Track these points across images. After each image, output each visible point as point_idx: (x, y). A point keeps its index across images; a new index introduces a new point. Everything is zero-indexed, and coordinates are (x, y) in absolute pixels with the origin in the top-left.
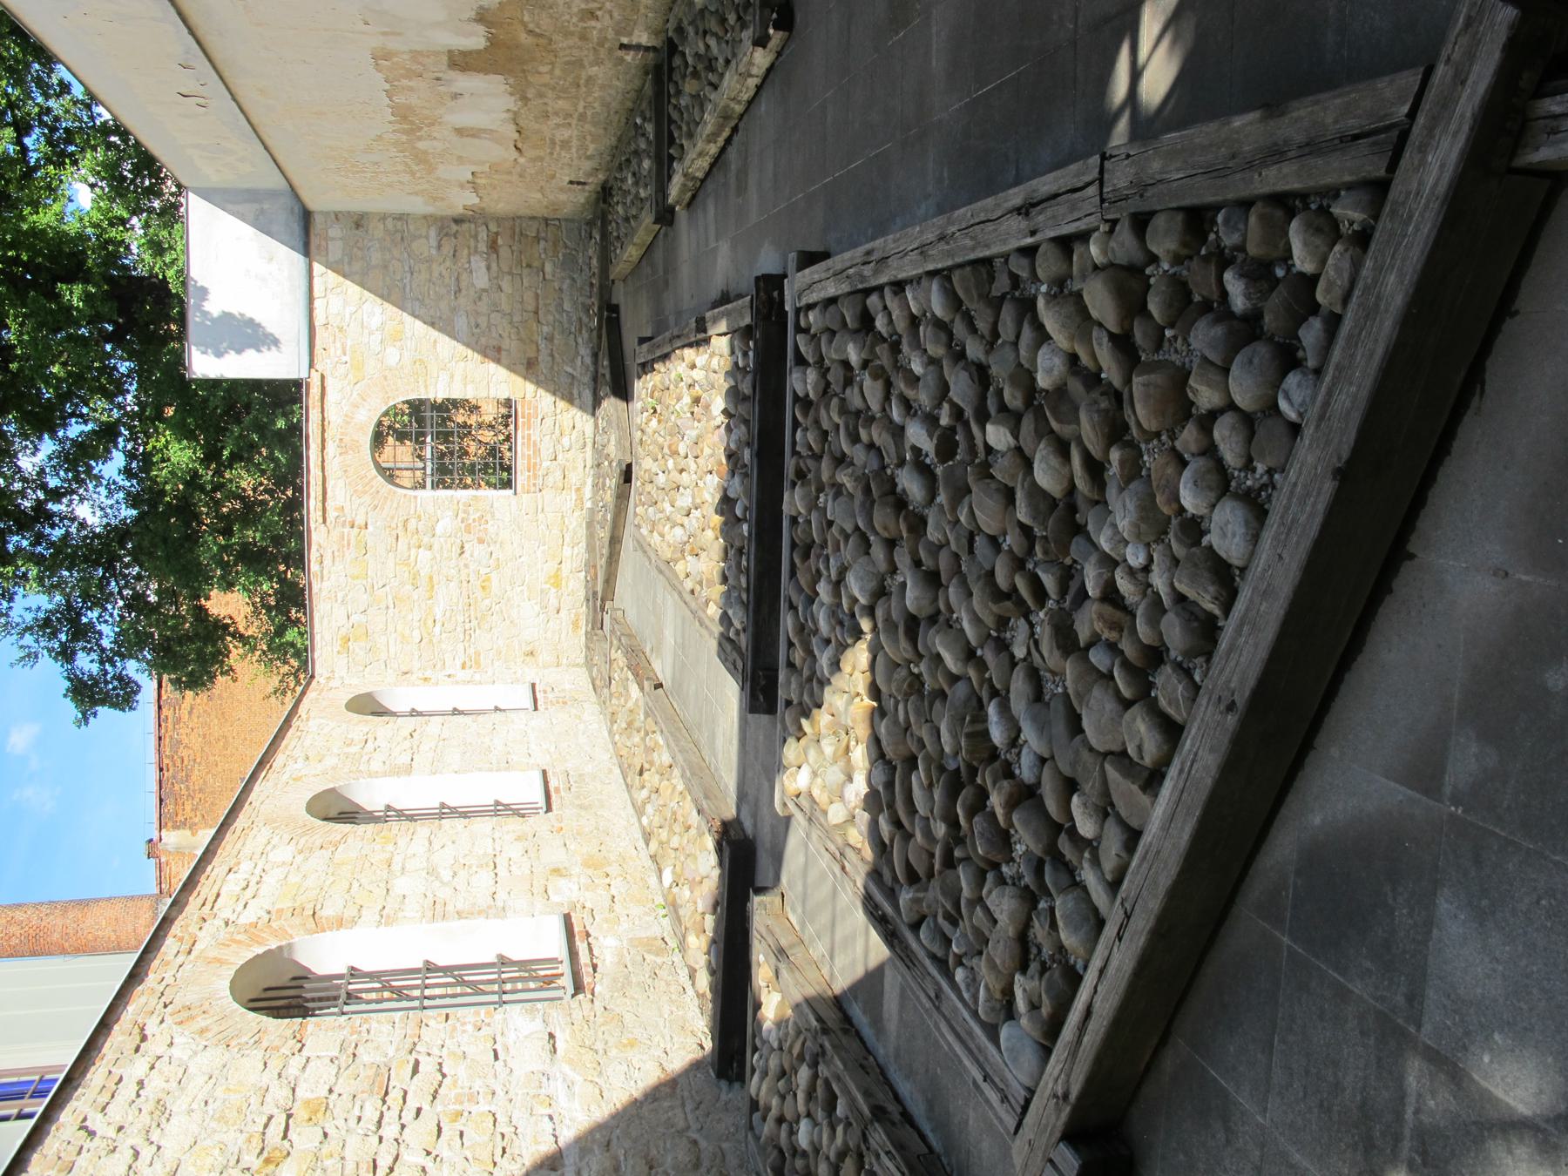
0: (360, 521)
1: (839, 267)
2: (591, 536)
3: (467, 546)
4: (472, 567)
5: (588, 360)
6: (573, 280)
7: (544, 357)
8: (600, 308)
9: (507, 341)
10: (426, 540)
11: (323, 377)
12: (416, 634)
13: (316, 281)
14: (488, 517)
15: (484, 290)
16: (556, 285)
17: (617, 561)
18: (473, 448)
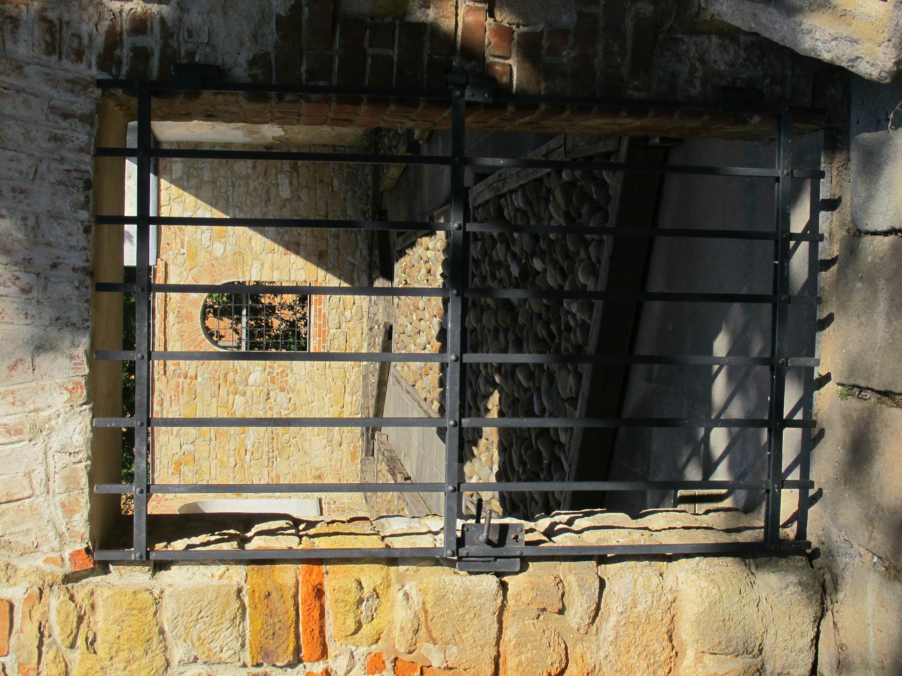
0: (191, 373)
1: (490, 182)
2: (365, 386)
3: (272, 393)
5: (365, 252)
6: (355, 192)
7: (332, 250)
8: (373, 213)
9: (304, 238)
10: (241, 388)
11: (166, 265)
12: (232, 460)
13: (163, 193)
14: (289, 371)
15: (287, 200)
16: (342, 196)
17: (384, 400)
18: (276, 323)
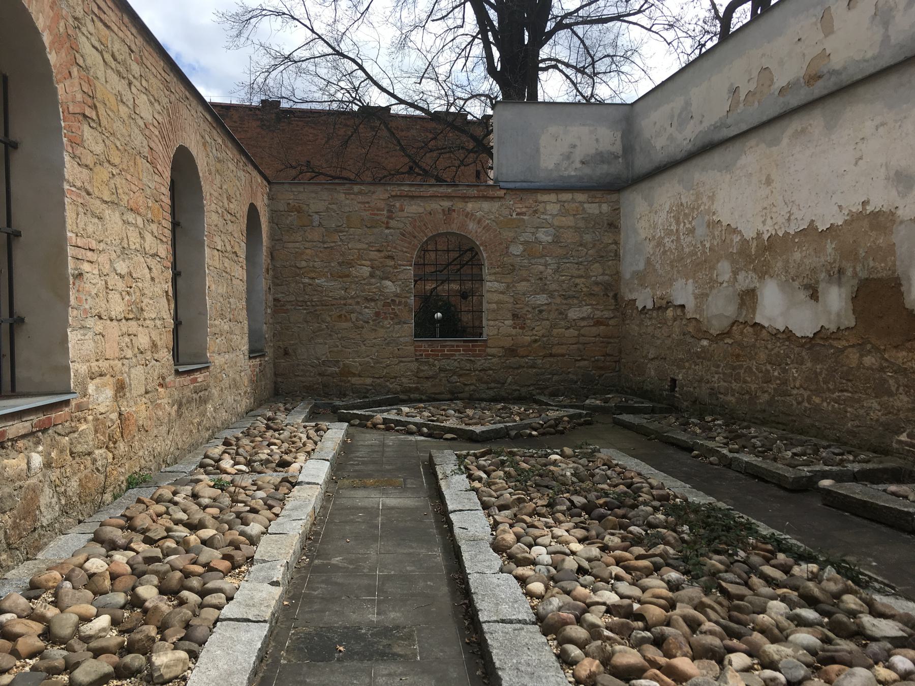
0: (393, 223)
4: (357, 308)
